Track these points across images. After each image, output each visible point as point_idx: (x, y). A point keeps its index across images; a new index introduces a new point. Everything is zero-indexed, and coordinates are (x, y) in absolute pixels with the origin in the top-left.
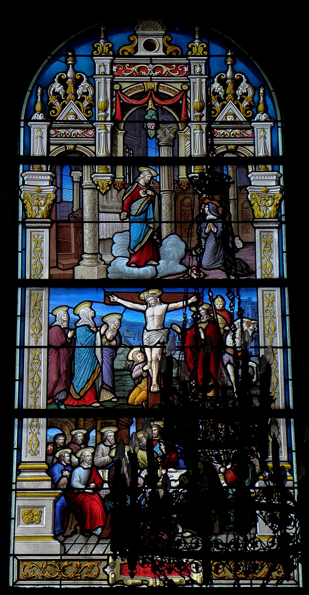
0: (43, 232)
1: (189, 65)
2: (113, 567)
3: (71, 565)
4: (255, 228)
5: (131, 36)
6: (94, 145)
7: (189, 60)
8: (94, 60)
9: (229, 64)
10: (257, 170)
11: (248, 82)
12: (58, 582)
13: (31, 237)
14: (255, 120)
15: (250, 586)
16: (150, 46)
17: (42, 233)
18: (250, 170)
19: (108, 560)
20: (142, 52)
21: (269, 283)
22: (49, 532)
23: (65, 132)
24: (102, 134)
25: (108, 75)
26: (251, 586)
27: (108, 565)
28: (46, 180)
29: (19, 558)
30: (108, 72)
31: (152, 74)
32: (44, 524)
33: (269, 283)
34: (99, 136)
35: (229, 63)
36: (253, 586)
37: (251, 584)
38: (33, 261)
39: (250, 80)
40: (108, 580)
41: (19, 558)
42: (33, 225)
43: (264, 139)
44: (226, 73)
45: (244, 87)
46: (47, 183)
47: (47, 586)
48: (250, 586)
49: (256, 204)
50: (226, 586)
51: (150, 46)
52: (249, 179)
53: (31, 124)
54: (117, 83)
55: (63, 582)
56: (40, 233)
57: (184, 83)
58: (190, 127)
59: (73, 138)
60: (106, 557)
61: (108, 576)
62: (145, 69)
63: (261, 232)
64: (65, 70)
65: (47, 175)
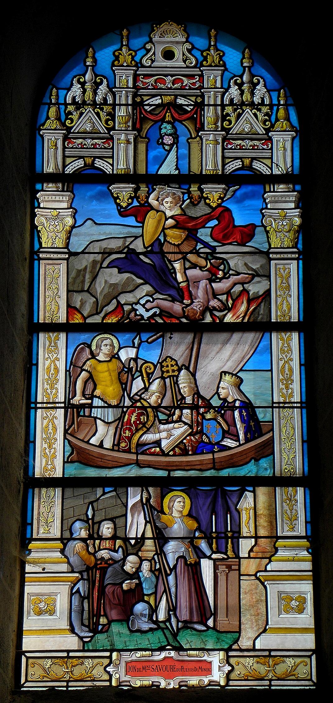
0: (290, 264)
1: (201, 76)
2: (117, 666)
3: (82, 663)
4: (39, 259)
5: (147, 43)
6: (112, 157)
7: (202, 71)
8: (114, 71)
9: (89, 66)
10: (272, 190)
11: (265, 86)
12: (65, 684)
13: (276, 271)
14: (45, 127)
15: (65, 689)
16: (169, 55)
17: (288, 266)
18: (267, 189)
19: (110, 657)
20: (161, 62)
21: (285, 327)
22: (65, 625)
23: (82, 143)
24: (122, 144)
25: (130, 88)
26: (67, 689)
27: (111, 662)
28: (291, 202)
29: (28, 655)
30: (131, 84)
31: (171, 87)
32: (58, 615)
33: (285, 327)
34: (118, 148)
35: (88, 64)
36: (272, 688)
37: (67, 686)
38: (279, 300)
39: (268, 84)
40: (110, 680)
41: (28, 655)
42: (286, 256)
43: (283, 153)
44: (84, 75)
45: (260, 90)
46: (292, 205)
47: (308, 688)
48: (65, 689)
49: (272, 229)
50: (239, 688)
51: (169, 55)
52: (265, 200)
53: (44, 133)
54: (141, 96)
55: (70, 684)
56: (287, 266)
57: (197, 96)
58: (200, 137)
59: (249, 149)
60: (108, 654)
61: (111, 676)
62: (164, 82)
63: (276, 264)
64: (95, 68)
65: (292, 196)
